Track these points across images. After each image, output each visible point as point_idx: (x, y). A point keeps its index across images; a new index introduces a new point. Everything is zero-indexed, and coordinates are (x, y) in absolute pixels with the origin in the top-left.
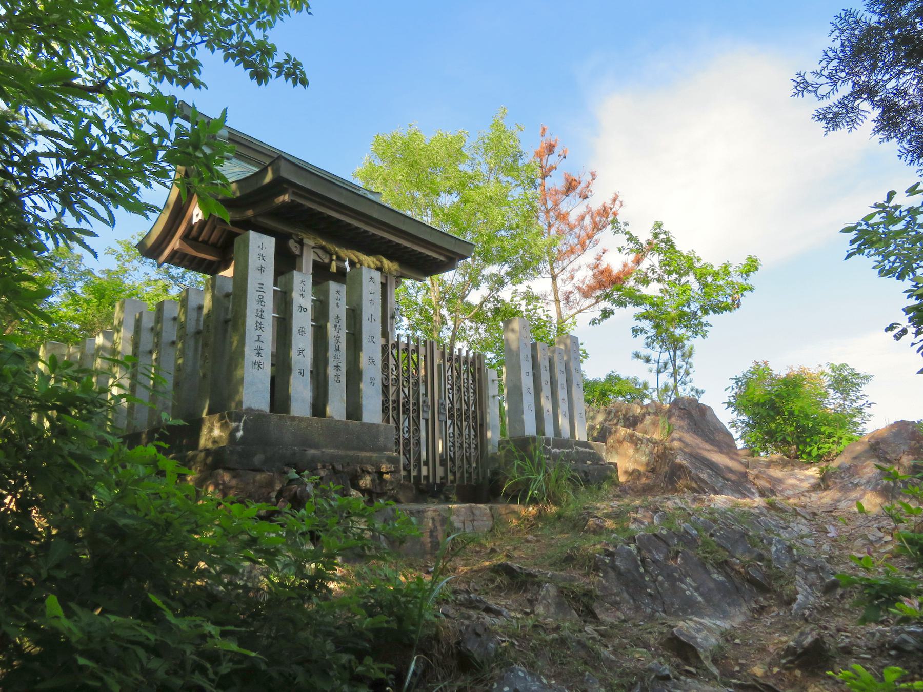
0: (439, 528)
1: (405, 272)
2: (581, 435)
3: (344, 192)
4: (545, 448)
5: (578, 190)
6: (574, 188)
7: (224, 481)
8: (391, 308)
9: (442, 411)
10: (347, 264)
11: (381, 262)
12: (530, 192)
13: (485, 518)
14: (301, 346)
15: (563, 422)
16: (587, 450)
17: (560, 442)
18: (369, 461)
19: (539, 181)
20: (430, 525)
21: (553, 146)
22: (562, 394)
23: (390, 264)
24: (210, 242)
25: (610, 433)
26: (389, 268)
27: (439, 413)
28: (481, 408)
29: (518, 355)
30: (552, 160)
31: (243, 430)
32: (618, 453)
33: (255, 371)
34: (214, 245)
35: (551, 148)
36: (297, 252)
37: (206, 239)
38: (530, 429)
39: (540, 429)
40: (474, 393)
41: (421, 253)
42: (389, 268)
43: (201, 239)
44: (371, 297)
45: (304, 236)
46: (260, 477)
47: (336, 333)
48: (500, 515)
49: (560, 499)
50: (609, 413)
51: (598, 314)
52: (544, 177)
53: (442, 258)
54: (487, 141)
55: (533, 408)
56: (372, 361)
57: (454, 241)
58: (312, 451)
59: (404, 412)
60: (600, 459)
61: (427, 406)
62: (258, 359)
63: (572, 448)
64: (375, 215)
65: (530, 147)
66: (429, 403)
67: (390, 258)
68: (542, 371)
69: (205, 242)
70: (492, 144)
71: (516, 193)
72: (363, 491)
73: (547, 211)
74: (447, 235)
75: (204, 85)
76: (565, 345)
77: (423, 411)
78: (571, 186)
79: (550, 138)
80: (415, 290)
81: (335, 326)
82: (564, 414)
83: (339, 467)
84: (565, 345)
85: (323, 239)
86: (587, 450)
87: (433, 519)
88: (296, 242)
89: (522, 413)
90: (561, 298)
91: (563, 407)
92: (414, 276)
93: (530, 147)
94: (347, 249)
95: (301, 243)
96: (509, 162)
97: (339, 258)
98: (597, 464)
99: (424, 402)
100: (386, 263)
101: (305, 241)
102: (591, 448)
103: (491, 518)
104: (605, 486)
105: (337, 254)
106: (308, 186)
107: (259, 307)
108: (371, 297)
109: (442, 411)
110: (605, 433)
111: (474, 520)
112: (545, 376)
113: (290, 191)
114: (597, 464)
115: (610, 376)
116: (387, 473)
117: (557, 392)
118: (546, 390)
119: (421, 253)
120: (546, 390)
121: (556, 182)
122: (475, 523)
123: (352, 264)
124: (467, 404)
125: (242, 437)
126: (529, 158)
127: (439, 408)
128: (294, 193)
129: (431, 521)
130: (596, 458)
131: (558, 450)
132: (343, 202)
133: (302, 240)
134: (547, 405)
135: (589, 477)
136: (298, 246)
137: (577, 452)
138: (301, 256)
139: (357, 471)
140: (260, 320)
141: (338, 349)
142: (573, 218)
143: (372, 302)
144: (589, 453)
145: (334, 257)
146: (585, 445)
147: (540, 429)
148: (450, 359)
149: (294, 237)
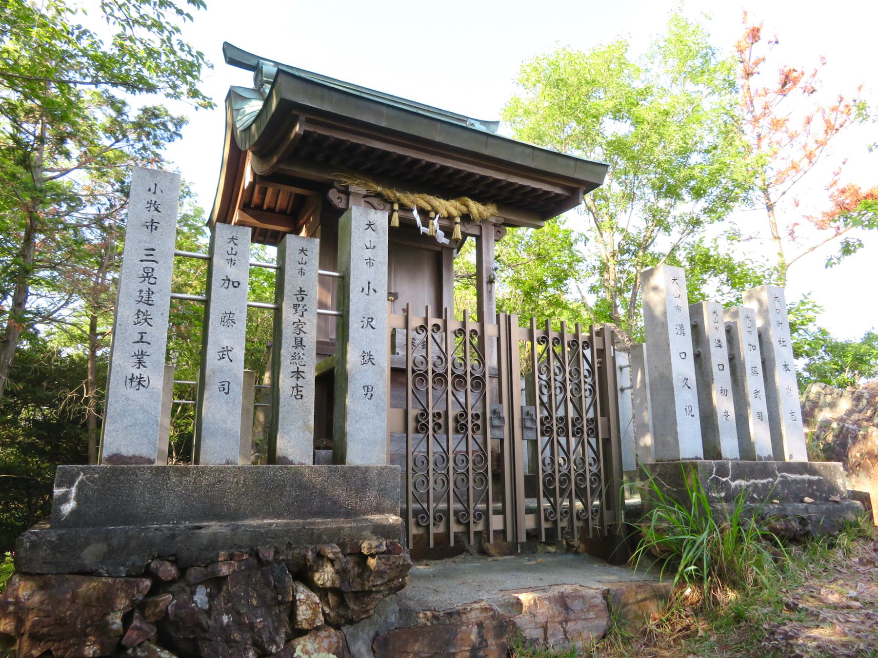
0: (491, 641)
1: (511, 217)
2: (796, 450)
3: (385, 110)
4: (716, 481)
5: (801, 84)
6: (795, 81)
7: (17, 598)
8: (488, 269)
9: (529, 424)
10: (415, 213)
11: (467, 206)
12: (727, 98)
13: (592, 615)
14: (226, 343)
15: (759, 433)
16: (806, 477)
17: (749, 463)
18: (334, 536)
19: (739, 82)
20: (473, 637)
21: (758, 30)
22: (754, 383)
23: (481, 208)
24: (277, 210)
25: (855, 438)
26: (480, 214)
27: (523, 427)
28: (605, 412)
29: (665, 325)
30: (759, 49)
31: (78, 498)
32: (869, 476)
33: (131, 392)
34: (282, 212)
35: (755, 35)
36: (342, 206)
37: (284, 207)
38: (690, 445)
39: (712, 450)
40: (592, 391)
41: (530, 188)
42: (480, 214)
43: (265, 207)
44: (368, 254)
45: (349, 182)
46: (88, 587)
47: (296, 318)
48: (626, 605)
49: (743, 579)
50: (858, 399)
51: (835, 248)
52: (748, 74)
53: (558, 191)
54: (662, 44)
55: (696, 411)
56: (368, 358)
57: (572, 163)
58: (214, 527)
59: (457, 431)
60: (833, 489)
61: (501, 419)
62: (137, 373)
63: (775, 477)
64: (438, 139)
65: (725, 40)
66: (505, 414)
67: (481, 199)
68: (713, 348)
69: (271, 210)
70: (671, 46)
71: (710, 104)
72: (323, 592)
73: (756, 120)
74: (559, 155)
75: (205, 6)
76: (760, 302)
77: (493, 427)
78: (787, 80)
79: (753, 23)
80: (518, 244)
81: (295, 306)
82: (760, 416)
83: (268, 554)
84: (760, 302)
85: (378, 183)
86: (806, 477)
87: (480, 625)
88: (339, 191)
89: (674, 422)
90: (783, 233)
91: (757, 405)
92: (525, 221)
93: (725, 40)
94: (413, 193)
95: (346, 193)
96: (697, 63)
97: (403, 207)
98: (827, 500)
99: (494, 412)
100: (475, 208)
101: (353, 189)
102: (812, 471)
103: (605, 614)
104: (843, 540)
105: (398, 200)
106: (327, 108)
107: (145, 286)
108: (368, 254)
109: (529, 424)
110: (845, 438)
111: (566, 622)
112: (718, 356)
113: (302, 118)
114: (827, 500)
115: (869, 334)
116: (373, 556)
117: (743, 380)
118: (721, 379)
119: (530, 188)
120: (721, 379)
121: (768, 78)
122: (571, 626)
123: (423, 212)
124: (578, 409)
125: (73, 512)
126: (726, 53)
127: (523, 420)
128: (309, 121)
129: (475, 630)
130: (824, 491)
131: (743, 483)
132: (384, 124)
133: (347, 187)
134: (723, 405)
135: (809, 527)
136: (343, 196)
137: (785, 483)
138: (347, 208)
139: (305, 557)
140: (144, 308)
141: (300, 343)
142: (795, 124)
143: (370, 262)
144: (810, 482)
145: (396, 207)
146: (802, 468)
147: (712, 450)
148: (544, 340)
149: (336, 184)
